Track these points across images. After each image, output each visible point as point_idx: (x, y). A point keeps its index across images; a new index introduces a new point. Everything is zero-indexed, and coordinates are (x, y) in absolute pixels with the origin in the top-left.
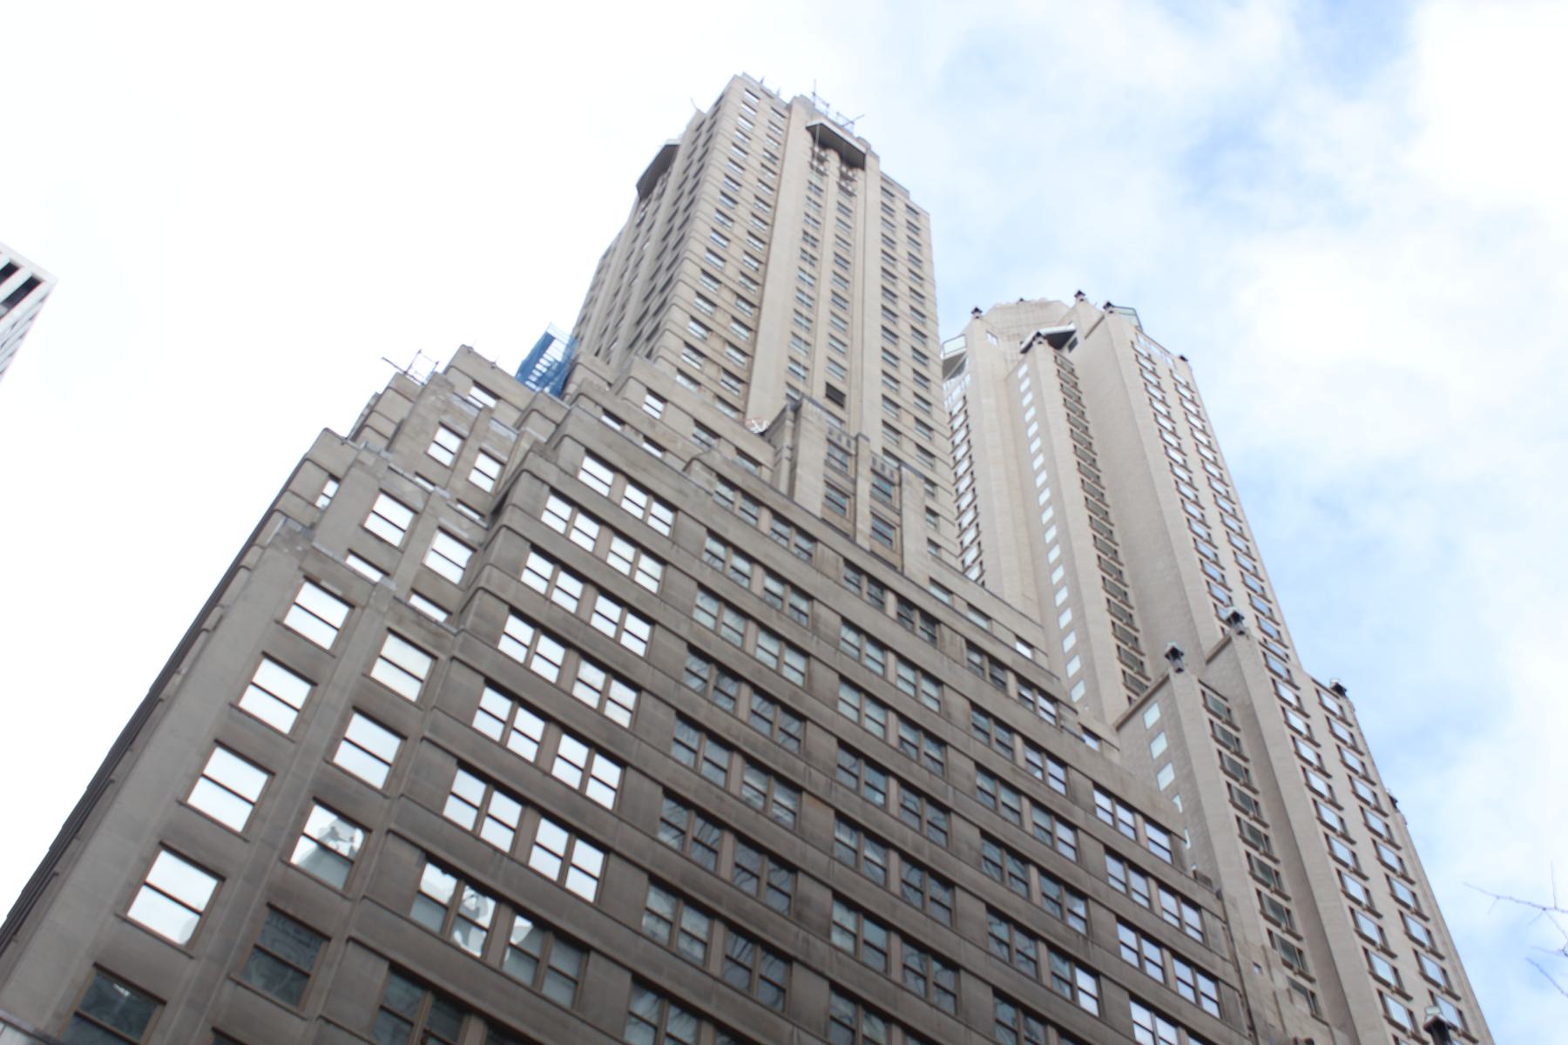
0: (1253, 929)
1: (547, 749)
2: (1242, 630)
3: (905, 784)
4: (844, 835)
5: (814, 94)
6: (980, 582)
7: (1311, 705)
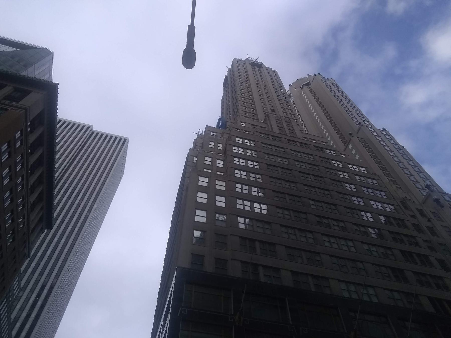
0: (386, 179)
1: (250, 190)
2: (362, 125)
3: (313, 175)
4: (306, 188)
5: (248, 57)
6: (308, 133)
7: (380, 135)
